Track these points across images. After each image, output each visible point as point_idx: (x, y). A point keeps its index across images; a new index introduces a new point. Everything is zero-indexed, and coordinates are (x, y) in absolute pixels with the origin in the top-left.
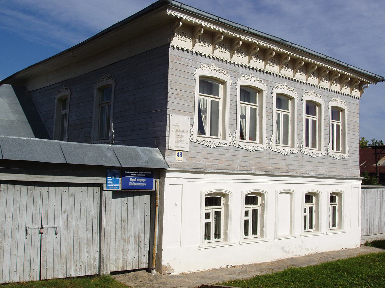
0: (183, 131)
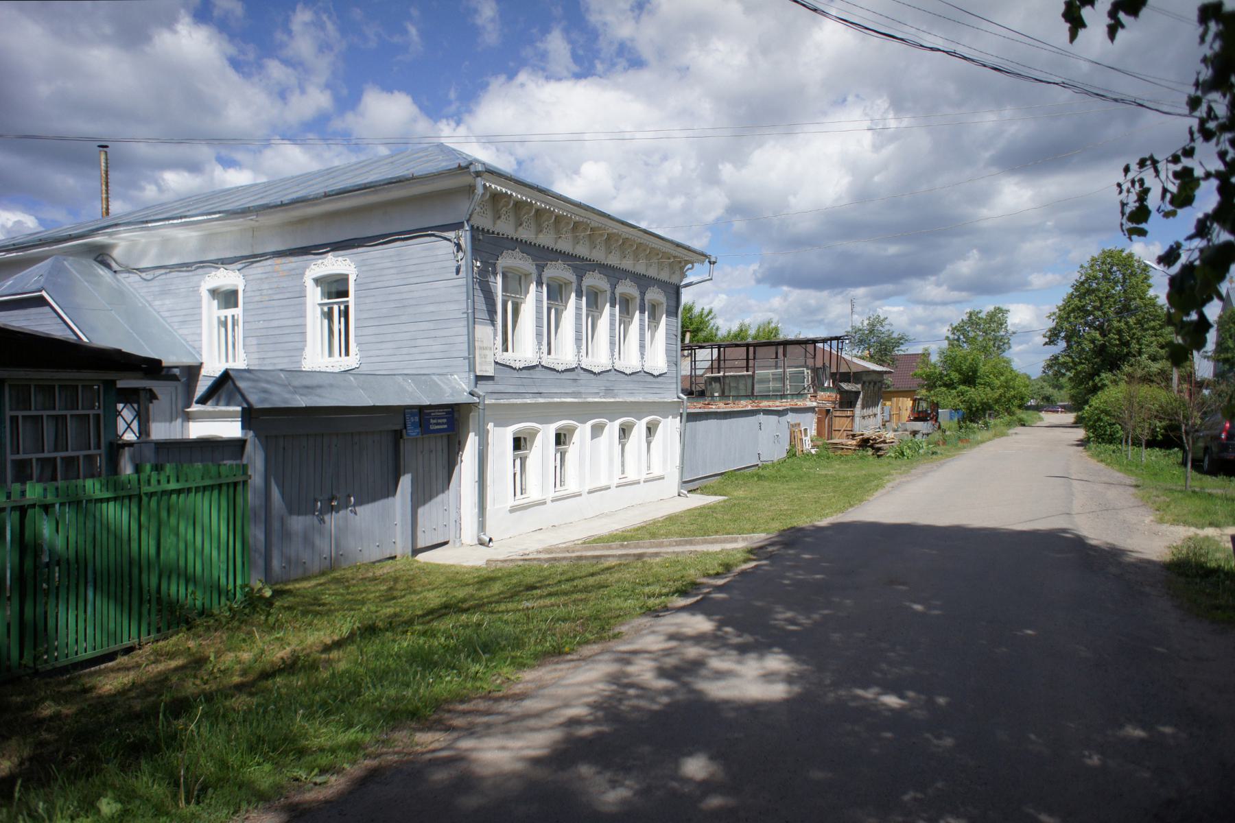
0: (486, 348)
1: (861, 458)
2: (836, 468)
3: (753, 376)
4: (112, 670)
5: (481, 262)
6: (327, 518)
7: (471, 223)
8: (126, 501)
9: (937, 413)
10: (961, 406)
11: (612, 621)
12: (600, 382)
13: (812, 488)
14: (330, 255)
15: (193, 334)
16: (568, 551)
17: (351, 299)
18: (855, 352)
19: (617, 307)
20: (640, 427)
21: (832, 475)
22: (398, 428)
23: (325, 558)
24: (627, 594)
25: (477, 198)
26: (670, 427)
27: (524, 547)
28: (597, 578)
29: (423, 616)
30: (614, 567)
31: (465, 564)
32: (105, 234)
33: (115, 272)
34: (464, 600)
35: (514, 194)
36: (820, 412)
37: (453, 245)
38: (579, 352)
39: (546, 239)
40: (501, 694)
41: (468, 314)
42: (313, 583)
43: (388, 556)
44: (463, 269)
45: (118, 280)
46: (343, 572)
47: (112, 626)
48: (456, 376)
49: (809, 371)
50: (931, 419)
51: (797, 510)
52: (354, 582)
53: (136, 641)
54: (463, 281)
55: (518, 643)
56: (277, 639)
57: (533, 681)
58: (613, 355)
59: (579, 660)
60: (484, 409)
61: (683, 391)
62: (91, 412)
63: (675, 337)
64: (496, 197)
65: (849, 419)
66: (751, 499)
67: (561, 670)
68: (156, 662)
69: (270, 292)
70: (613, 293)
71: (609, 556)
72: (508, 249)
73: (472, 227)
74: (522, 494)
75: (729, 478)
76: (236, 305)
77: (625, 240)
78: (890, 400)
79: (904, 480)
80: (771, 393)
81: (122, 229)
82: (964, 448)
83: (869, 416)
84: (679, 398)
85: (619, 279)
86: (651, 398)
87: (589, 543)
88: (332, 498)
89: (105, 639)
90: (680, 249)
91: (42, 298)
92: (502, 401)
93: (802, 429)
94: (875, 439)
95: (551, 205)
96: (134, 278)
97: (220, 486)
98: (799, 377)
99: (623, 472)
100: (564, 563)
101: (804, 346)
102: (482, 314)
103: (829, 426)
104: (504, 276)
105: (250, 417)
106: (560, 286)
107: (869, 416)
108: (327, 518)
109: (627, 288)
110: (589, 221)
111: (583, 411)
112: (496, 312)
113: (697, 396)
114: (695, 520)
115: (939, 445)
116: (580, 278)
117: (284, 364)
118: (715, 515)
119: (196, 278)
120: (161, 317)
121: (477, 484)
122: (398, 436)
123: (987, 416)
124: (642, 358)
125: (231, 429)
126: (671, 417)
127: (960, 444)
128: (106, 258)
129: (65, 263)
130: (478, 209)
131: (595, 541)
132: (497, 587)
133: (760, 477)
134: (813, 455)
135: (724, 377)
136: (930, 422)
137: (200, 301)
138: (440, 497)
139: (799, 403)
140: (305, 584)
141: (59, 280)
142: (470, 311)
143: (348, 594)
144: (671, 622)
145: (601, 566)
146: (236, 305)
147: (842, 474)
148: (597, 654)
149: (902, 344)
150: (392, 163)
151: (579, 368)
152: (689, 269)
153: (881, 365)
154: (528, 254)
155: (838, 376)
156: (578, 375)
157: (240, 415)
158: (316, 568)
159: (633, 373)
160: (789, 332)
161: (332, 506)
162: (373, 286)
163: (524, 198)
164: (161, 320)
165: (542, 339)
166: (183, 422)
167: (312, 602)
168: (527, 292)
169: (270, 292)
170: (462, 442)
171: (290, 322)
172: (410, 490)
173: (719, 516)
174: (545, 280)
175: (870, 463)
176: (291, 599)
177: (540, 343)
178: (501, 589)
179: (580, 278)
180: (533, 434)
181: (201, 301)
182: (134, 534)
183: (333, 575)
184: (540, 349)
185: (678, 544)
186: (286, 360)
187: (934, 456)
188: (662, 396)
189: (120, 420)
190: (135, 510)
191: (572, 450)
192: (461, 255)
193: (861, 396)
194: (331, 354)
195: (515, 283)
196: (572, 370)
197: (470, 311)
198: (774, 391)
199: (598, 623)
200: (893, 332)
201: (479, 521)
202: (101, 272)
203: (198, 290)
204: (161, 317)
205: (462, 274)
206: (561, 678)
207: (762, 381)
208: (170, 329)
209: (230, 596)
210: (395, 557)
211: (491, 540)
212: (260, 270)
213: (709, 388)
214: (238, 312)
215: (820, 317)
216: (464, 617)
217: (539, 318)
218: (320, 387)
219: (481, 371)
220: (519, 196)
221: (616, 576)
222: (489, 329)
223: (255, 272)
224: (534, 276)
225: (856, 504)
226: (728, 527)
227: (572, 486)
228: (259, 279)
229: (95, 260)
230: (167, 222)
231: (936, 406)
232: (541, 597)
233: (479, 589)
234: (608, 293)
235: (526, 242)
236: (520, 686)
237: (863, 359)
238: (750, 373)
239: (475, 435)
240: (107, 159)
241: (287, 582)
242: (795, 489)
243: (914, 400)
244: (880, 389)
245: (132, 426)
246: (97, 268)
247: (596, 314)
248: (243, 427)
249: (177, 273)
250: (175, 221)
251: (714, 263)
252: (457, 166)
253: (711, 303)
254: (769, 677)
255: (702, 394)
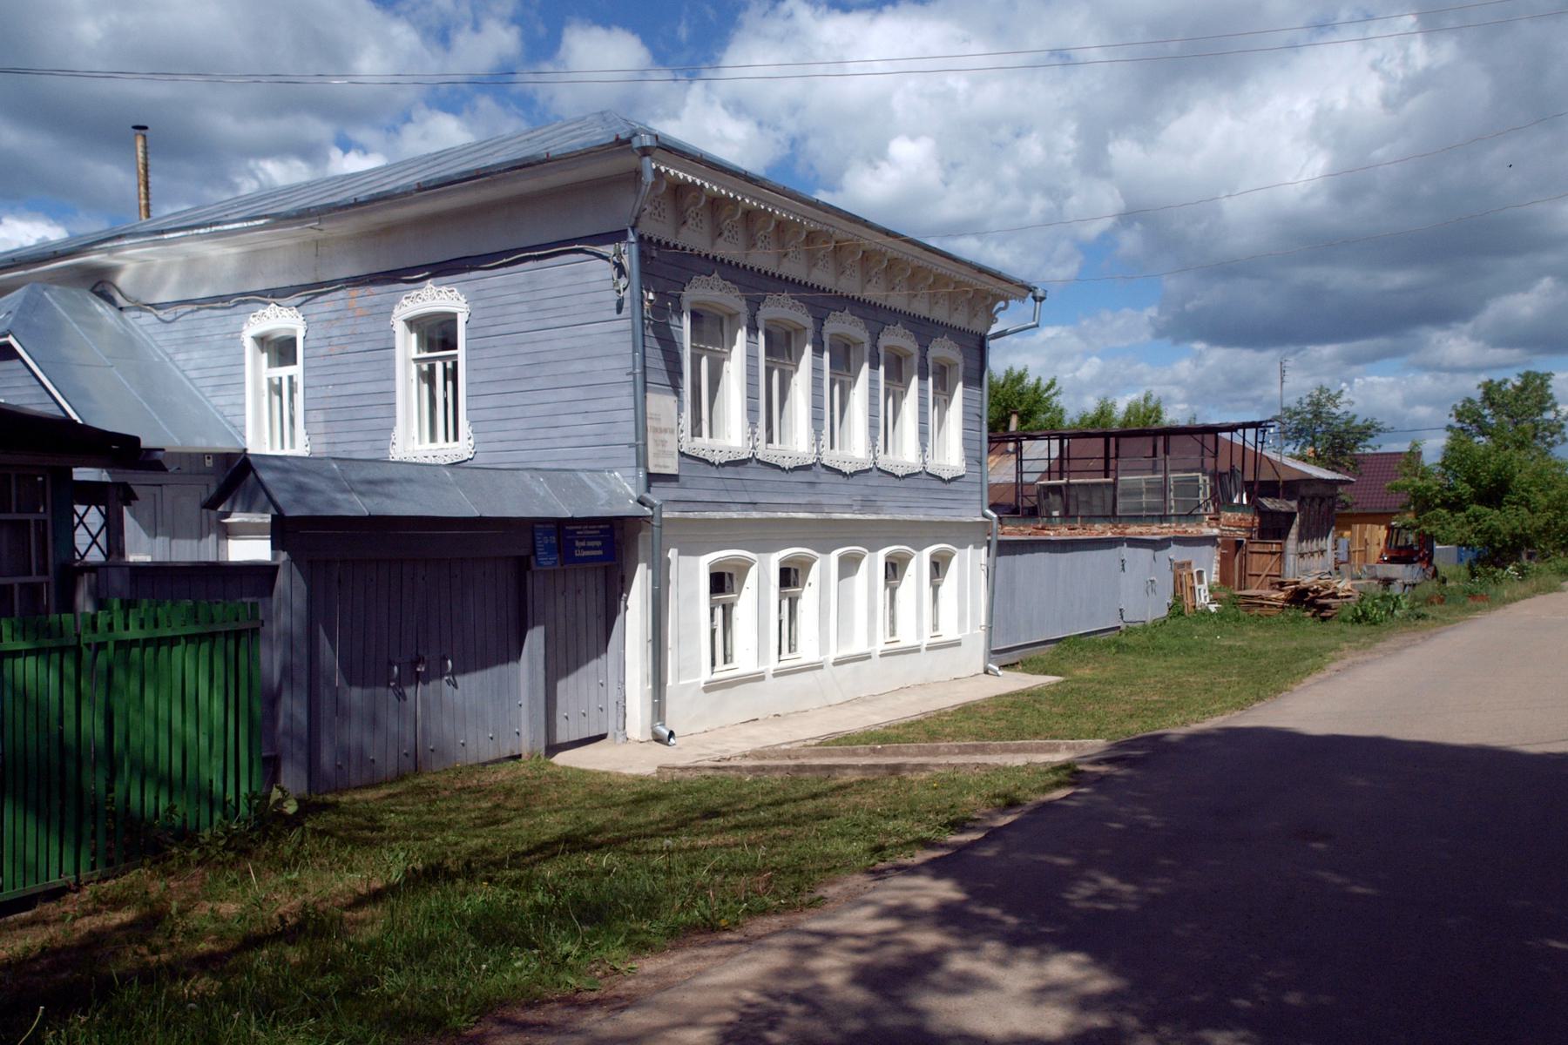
0: (666, 431)
1: (1293, 620)
2: (1252, 637)
3: (1114, 485)
4: (23, 925)
5: (655, 293)
6: (409, 691)
7: (638, 230)
8: (55, 657)
9: (1432, 550)
10: (1475, 540)
11: (817, 878)
12: (856, 488)
13: (1205, 667)
14: (429, 284)
15: (233, 404)
16: (789, 757)
17: (461, 352)
18: (1290, 449)
19: (930, 380)
20: (919, 563)
21: (1240, 648)
22: (523, 552)
23: (406, 755)
24: (856, 831)
25: (646, 189)
26: (970, 563)
27: (724, 747)
28: (820, 802)
29: (529, 853)
30: (851, 785)
31: (626, 771)
32: (102, 251)
33: (121, 309)
34: (597, 831)
35: (707, 185)
36: (1225, 544)
37: (610, 266)
38: (818, 440)
39: (762, 258)
40: (594, 995)
41: (634, 375)
42: (384, 792)
43: (508, 755)
44: (627, 304)
45: (124, 322)
46: (432, 777)
47: (31, 852)
48: (616, 474)
49: (1207, 478)
50: (1421, 560)
51: (1172, 702)
52: (447, 793)
53: (72, 878)
54: (626, 324)
55: (649, 906)
56: (288, 882)
57: (656, 975)
58: (874, 446)
59: (741, 942)
60: (660, 527)
61: (993, 507)
62: (32, 517)
63: (978, 419)
64: (679, 190)
65: (1275, 558)
66: (1099, 682)
67: (705, 959)
68: (97, 912)
69: (343, 340)
70: (875, 346)
71: (847, 767)
72: (700, 274)
73: (641, 238)
74: (725, 662)
75: (1065, 650)
76: (295, 363)
77: (893, 262)
78: (1349, 528)
79: (1360, 658)
80: (1144, 513)
81: (126, 242)
82: (1478, 609)
83: (1312, 554)
84: (984, 516)
85: (884, 324)
86: (938, 515)
87: (827, 744)
88: (419, 660)
89: (19, 873)
90: (984, 278)
91: (9, 345)
92: (691, 515)
93: (1195, 571)
94: (1316, 591)
95: (768, 203)
96: (147, 318)
97: (213, 636)
98: (1190, 487)
99: (893, 633)
100: (777, 775)
101: (1199, 437)
102: (659, 376)
103: (1241, 567)
104: (696, 317)
105: (283, 531)
106: (788, 334)
107: (1312, 554)
108: (409, 691)
109: (897, 338)
110: (831, 230)
111: (826, 534)
112: (681, 374)
113: (1024, 516)
114: (1006, 713)
115: (1432, 603)
116: (820, 322)
117: (362, 451)
118: (1037, 706)
119: (235, 320)
120: (186, 376)
121: (650, 645)
122: (522, 566)
123: (1524, 557)
124: (924, 451)
125: (252, 550)
126: (971, 547)
127: (1470, 603)
128: (107, 287)
129: (46, 294)
130: (649, 209)
131: (837, 742)
132: (658, 811)
133: (1121, 648)
134: (1212, 614)
135: (1068, 485)
136: (1417, 566)
137: (243, 354)
138: (593, 664)
139: (1190, 530)
140: (371, 795)
141: (35, 320)
142: (638, 371)
143: (430, 812)
144: (896, 891)
145: (833, 783)
146: (295, 363)
147: (1258, 646)
148: (774, 933)
149: (1372, 436)
150: (528, 140)
151: (754, 460)
152: (1000, 309)
153: (1333, 470)
154: (733, 282)
155: (1256, 487)
156: (818, 477)
157: (269, 529)
158: (390, 768)
159: (908, 476)
160: (1175, 415)
161: (418, 672)
162: (493, 331)
163: (723, 192)
164: (187, 383)
165: (757, 418)
166: (218, 538)
167: (365, 823)
168: (733, 342)
169: (343, 340)
170: (626, 580)
171: (372, 388)
172: (542, 651)
173: (1045, 708)
174: (761, 325)
175: (1310, 632)
176: (333, 817)
177: (753, 423)
178: (665, 814)
179: (820, 322)
180: (744, 567)
181: (243, 354)
182: (70, 707)
183: (417, 781)
184: (753, 433)
185: (963, 751)
186: (367, 446)
187: (1421, 622)
188: (954, 512)
189: (80, 531)
190: (69, 668)
191: (808, 597)
192: (623, 282)
193: (1297, 519)
194: (433, 438)
195: (713, 329)
196: (807, 468)
197: (638, 371)
198: (1148, 509)
199: (795, 879)
200: (1355, 417)
201: (654, 703)
202: (100, 309)
203: (239, 337)
204: (186, 376)
205: (626, 312)
206: (700, 973)
207: (1128, 493)
208: (201, 397)
209: (229, 811)
210: (520, 756)
211: (672, 734)
212: (330, 307)
213: (1044, 503)
214: (296, 370)
215: (1256, 393)
216: (589, 858)
217: (751, 385)
218: (390, 481)
219: (656, 466)
220: (715, 188)
221: (853, 799)
222: (671, 400)
223: (320, 310)
224: (744, 318)
225: (1268, 696)
226: (1056, 727)
227: (807, 650)
228: (326, 321)
229: (93, 290)
230: (190, 232)
231: (1427, 541)
232: (722, 830)
233: (628, 814)
234: (867, 347)
235: (722, 260)
236: (631, 983)
237: (1305, 461)
238: (1110, 480)
239: (648, 568)
240: (145, 147)
241: (340, 791)
242: (1176, 669)
243: (1390, 529)
244: (1331, 509)
245: (99, 540)
246: (93, 302)
247: (847, 379)
248: (273, 548)
249: (208, 311)
250: (202, 231)
251: (1042, 299)
252: (613, 139)
253: (1077, 369)
254: (1044, 993)
255: (1033, 513)
